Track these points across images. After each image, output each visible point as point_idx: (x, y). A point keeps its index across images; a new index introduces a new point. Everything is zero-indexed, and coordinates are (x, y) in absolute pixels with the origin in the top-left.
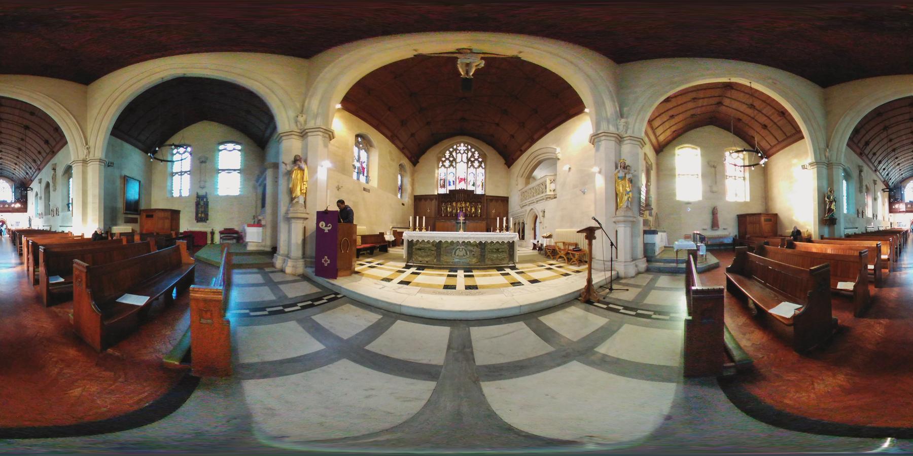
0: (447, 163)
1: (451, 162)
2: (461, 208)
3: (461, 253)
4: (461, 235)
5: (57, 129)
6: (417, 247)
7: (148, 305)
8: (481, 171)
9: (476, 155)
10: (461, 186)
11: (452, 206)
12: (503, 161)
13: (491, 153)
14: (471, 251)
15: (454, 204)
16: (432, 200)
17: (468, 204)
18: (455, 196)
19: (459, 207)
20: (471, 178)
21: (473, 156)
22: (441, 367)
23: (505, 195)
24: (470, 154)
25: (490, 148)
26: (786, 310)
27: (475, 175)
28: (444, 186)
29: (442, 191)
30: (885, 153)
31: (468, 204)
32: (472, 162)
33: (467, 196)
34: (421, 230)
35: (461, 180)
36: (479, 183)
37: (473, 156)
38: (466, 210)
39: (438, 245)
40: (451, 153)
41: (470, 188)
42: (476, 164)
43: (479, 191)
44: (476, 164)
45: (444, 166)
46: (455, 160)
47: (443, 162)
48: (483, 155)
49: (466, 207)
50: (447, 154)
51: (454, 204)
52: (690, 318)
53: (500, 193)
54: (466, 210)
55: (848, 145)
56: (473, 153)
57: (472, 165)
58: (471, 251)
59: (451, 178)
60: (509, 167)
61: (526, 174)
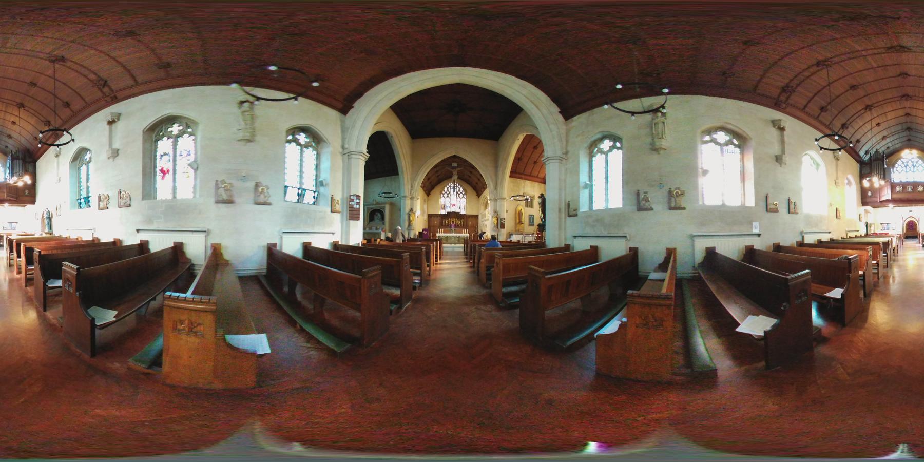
0: (446, 195)
4: (453, 234)
5: (473, 167)
7: (819, 330)
8: (464, 200)
10: (453, 210)
13: (469, 189)
18: (450, 215)
19: (452, 221)
20: (458, 205)
22: (155, 198)
26: (754, 325)
29: (443, 212)
30: (893, 130)
33: (456, 215)
36: (463, 207)
39: (447, 237)
41: (458, 211)
43: (463, 212)
48: (464, 190)
52: (738, 329)
55: (510, 176)
59: (447, 204)
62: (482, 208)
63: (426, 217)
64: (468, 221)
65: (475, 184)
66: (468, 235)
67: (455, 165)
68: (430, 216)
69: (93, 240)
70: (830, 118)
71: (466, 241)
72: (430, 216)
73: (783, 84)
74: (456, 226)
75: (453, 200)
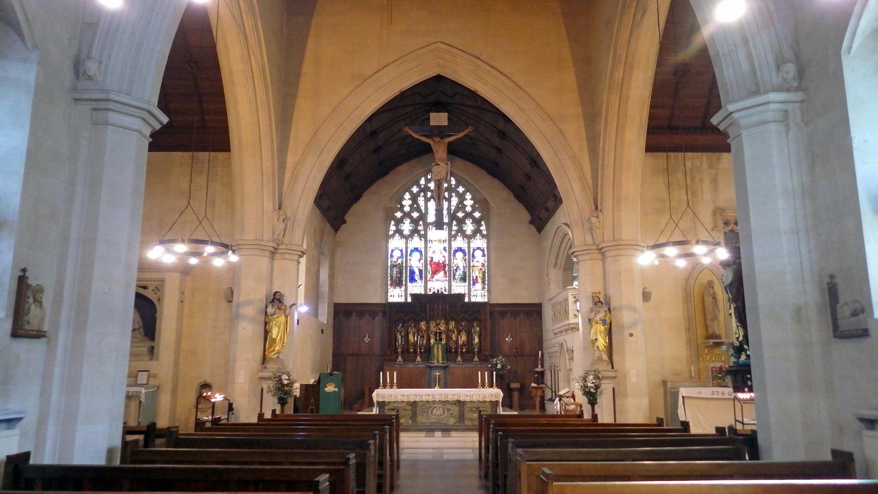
1: (415, 222)
2: (438, 335)
3: (437, 412)
4: (437, 393)
6: (390, 406)
9: (469, 203)
10: (438, 284)
11: (419, 330)
12: (525, 216)
13: (499, 195)
14: (449, 410)
15: (423, 325)
16: (373, 315)
17: (452, 325)
18: (425, 307)
21: (461, 206)
23: (535, 301)
24: (455, 201)
25: (496, 183)
27: (469, 256)
28: (398, 283)
29: (396, 296)
31: (452, 325)
32: (461, 222)
33: (449, 306)
34: (391, 387)
35: (438, 267)
37: (461, 206)
38: (449, 338)
40: (414, 198)
41: (459, 288)
42: (469, 227)
43: (478, 295)
44: (469, 227)
45: (399, 232)
46: (423, 217)
47: (399, 222)
48: (481, 203)
49: (448, 332)
50: (407, 203)
51: (423, 325)
53: (524, 297)
54: (449, 338)
55: (650, 148)
56: (462, 198)
57: (461, 231)
58: (449, 410)
59: (415, 262)
60: (540, 229)
61: (562, 261)
62: (555, 275)
63: (325, 316)
64: (498, 337)
65: (514, 177)
66: (495, 393)
67: (439, 119)
68: (343, 313)
69: (169, 428)
70: (701, 366)
71: (489, 425)
72: (343, 313)
73: (717, 332)
74: (450, 353)
75: (437, 246)
